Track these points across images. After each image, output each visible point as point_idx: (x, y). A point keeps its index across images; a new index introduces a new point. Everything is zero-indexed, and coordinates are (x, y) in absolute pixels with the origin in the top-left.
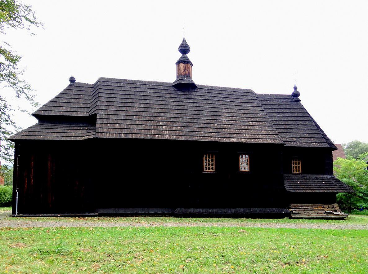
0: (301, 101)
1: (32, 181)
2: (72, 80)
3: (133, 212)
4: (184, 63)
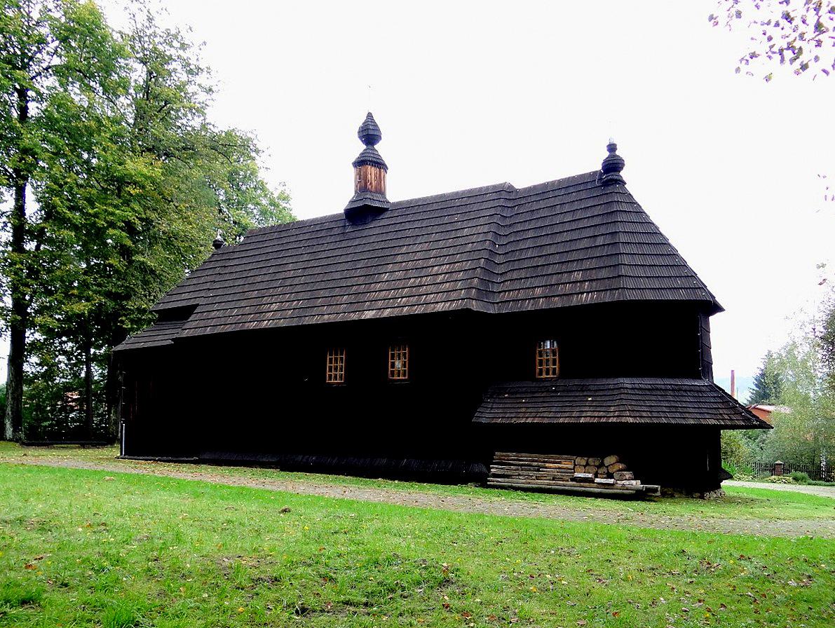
3: (234, 458)
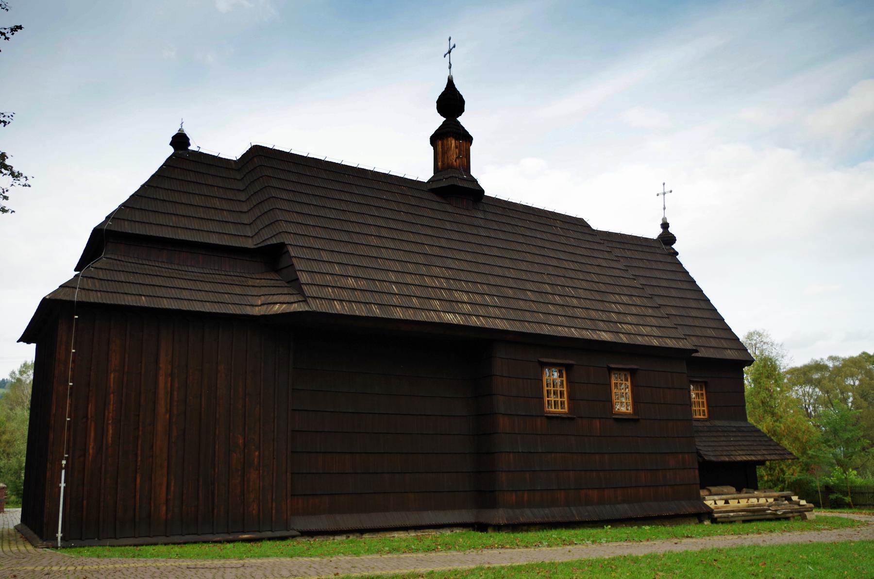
0: (677, 254)
1: (111, 431)
2: (180, 141)
4: (456, 139)
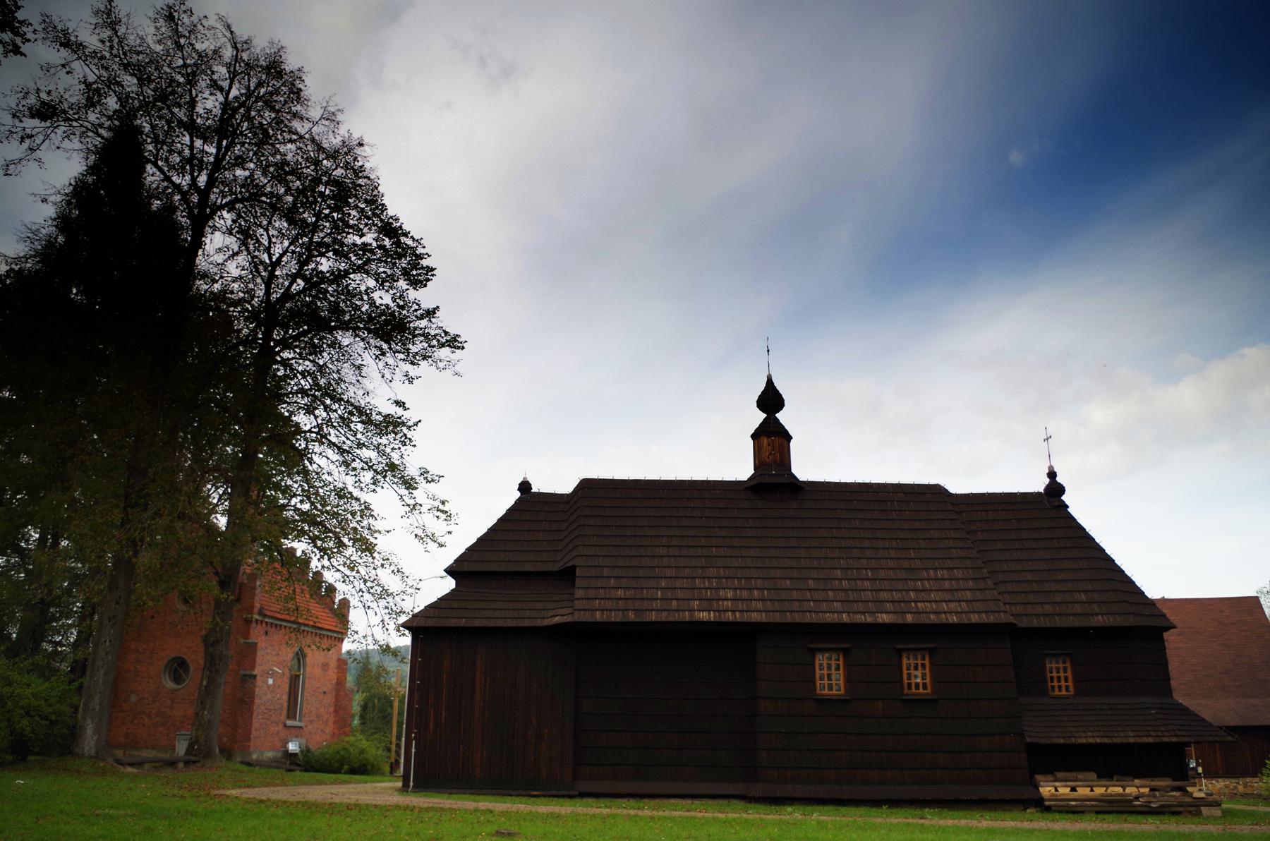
2: (525, 487)
4: (769, 437)
